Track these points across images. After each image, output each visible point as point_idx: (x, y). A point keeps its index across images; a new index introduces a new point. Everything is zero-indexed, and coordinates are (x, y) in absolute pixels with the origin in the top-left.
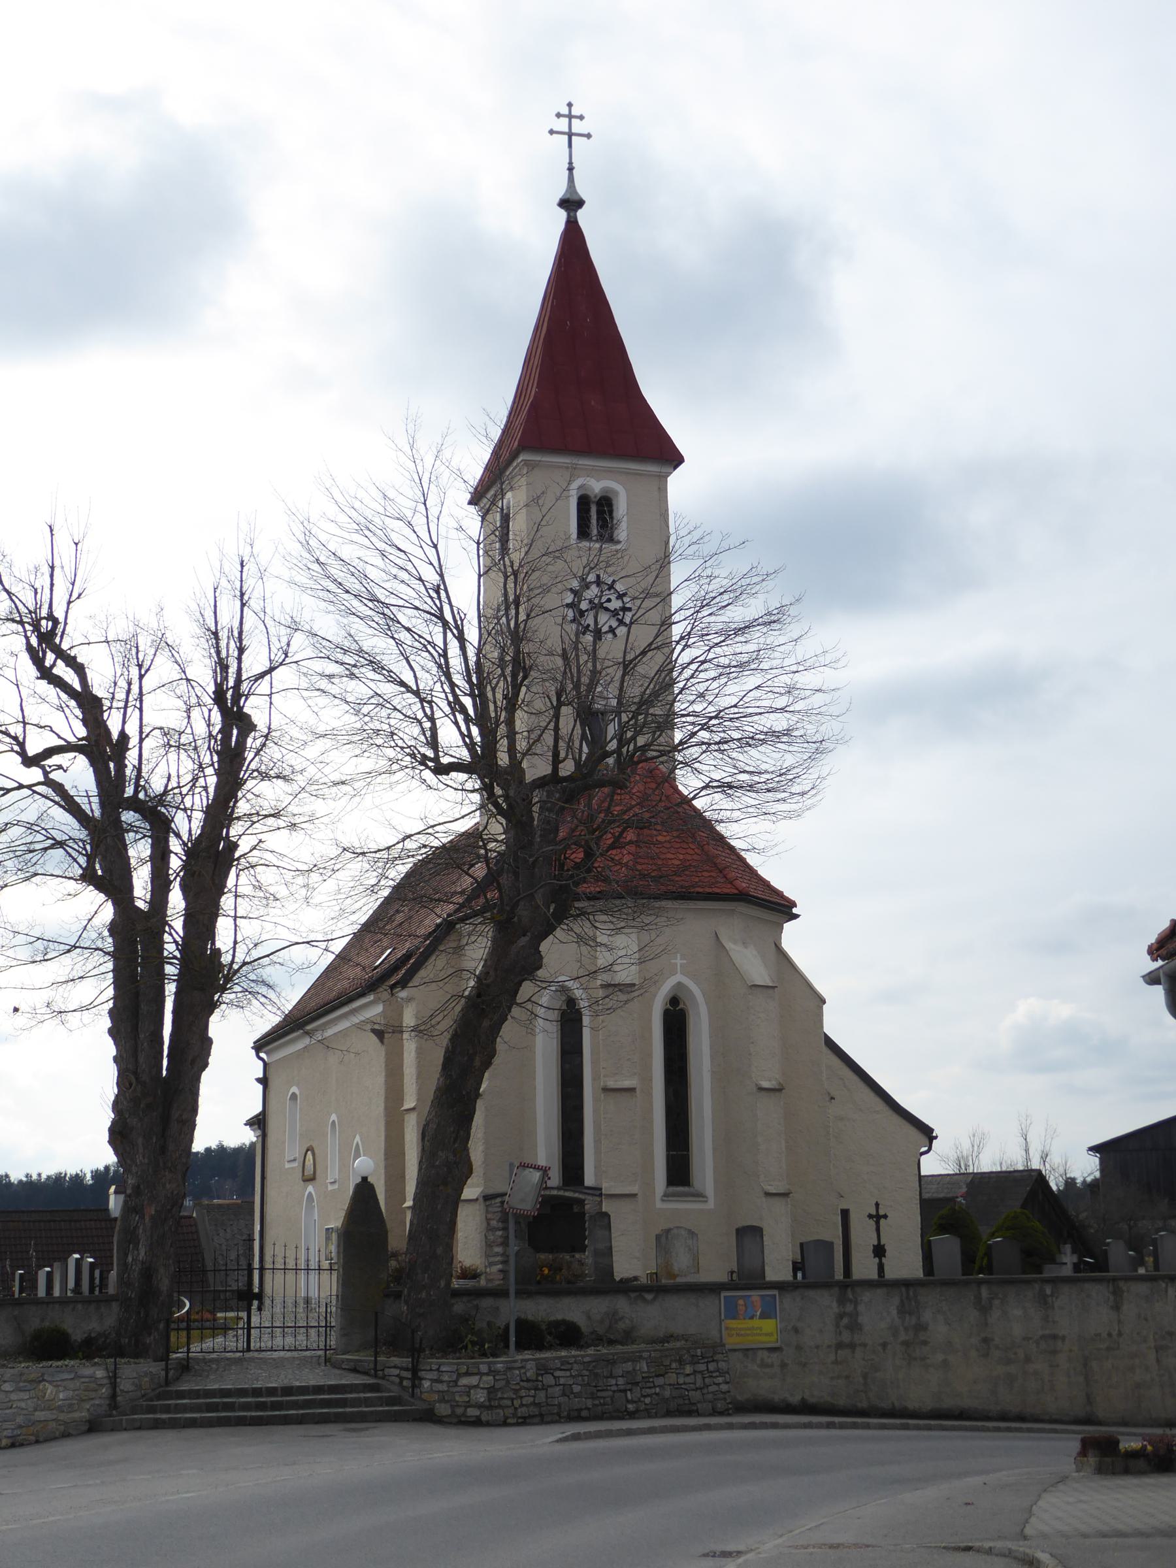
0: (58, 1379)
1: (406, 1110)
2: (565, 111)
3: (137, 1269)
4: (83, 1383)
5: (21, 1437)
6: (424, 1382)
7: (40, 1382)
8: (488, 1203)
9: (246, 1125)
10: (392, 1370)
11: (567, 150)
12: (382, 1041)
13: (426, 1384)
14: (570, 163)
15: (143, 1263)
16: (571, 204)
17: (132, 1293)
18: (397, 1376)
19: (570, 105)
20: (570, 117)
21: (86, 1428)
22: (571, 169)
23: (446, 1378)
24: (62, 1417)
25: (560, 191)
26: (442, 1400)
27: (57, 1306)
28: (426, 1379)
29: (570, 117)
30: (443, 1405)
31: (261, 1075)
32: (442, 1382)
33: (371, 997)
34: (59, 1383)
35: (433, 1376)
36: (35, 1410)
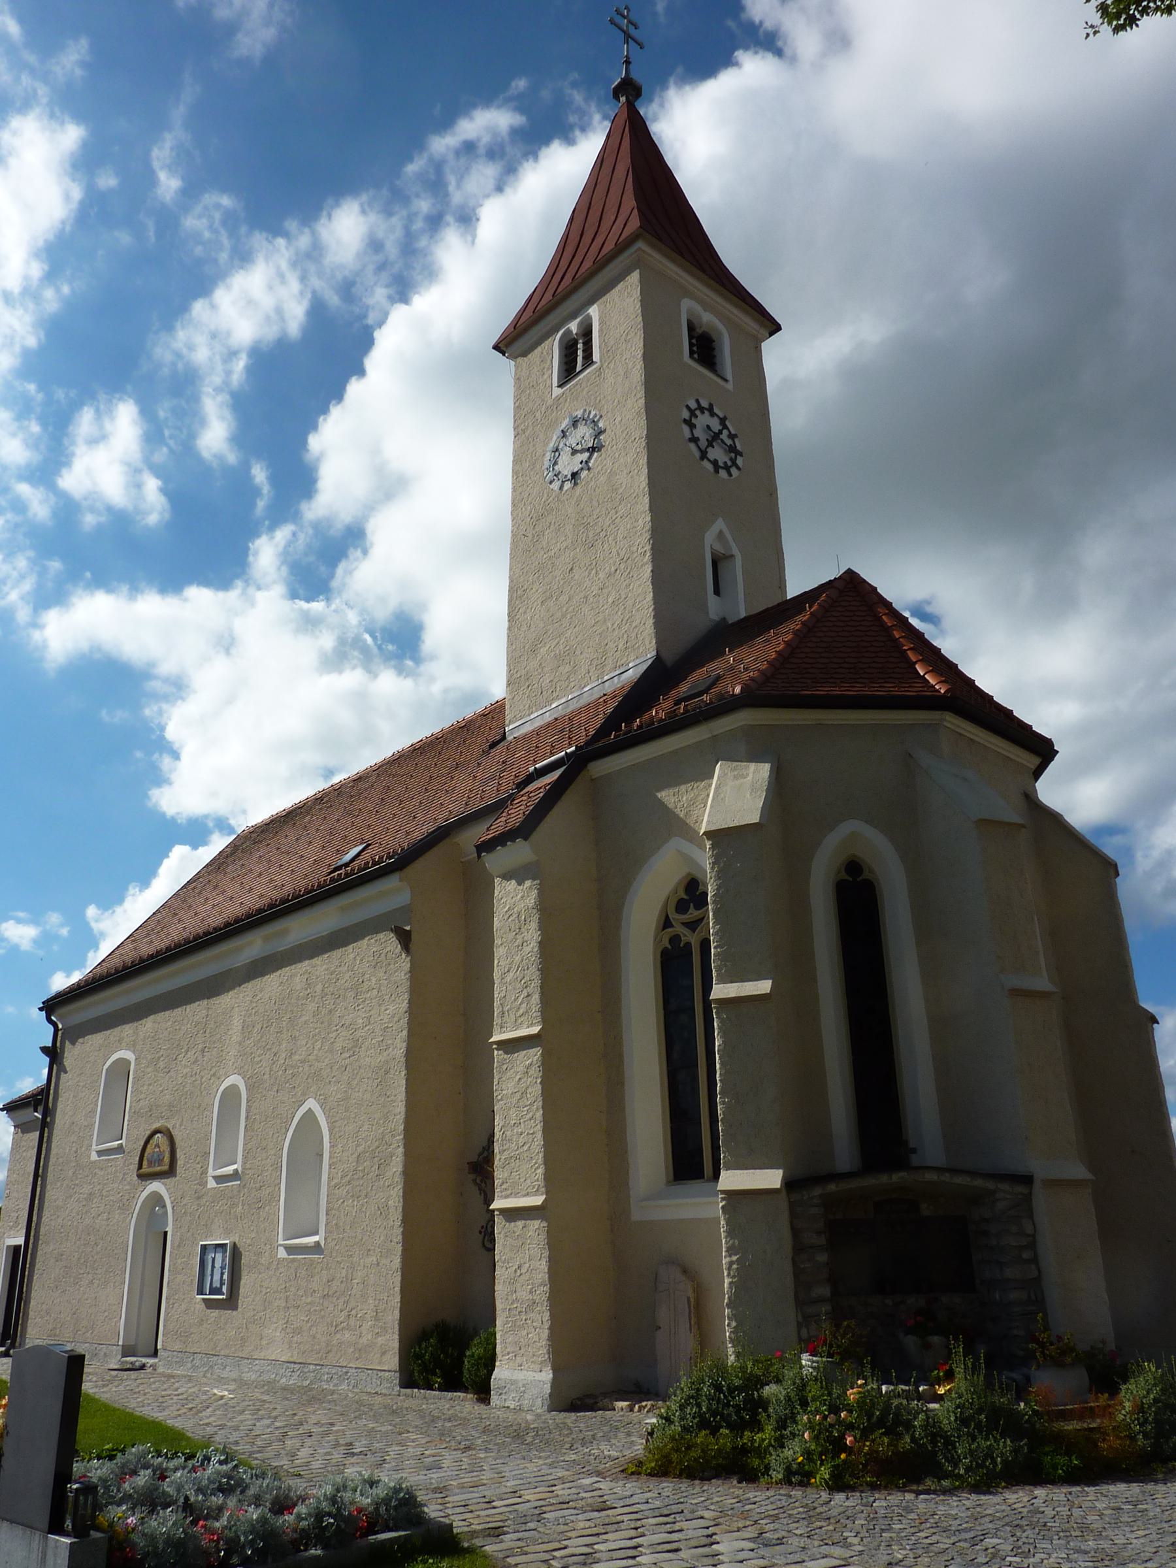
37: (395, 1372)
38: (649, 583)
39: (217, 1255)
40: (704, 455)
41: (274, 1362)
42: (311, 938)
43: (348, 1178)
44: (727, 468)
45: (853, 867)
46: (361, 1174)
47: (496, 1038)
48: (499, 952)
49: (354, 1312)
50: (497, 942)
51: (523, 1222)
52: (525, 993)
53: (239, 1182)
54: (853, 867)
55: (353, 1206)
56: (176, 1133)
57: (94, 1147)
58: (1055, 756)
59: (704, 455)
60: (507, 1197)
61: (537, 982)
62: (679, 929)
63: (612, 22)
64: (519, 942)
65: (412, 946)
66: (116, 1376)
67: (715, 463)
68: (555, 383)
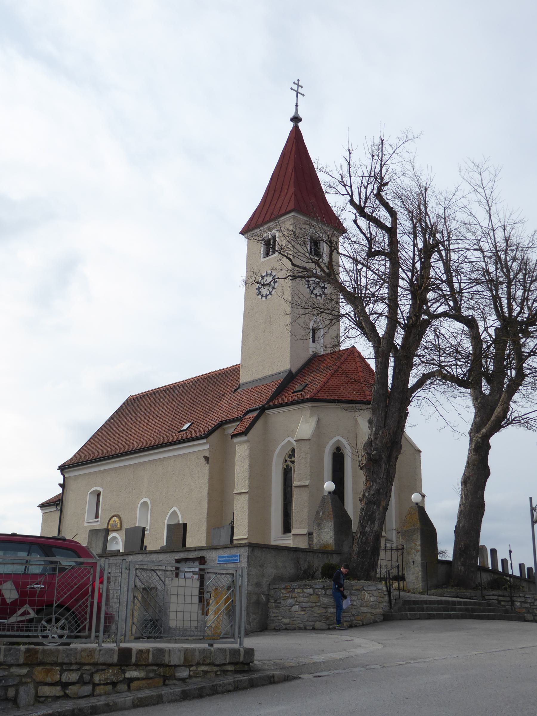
0: (370, 590)
1: (235, 493)
2: (297, 82)
3: (372, 535)
4: (380, 593)
5: (355, 622)
6: (516, 603)
7: (362, 590)
8: (310, 536)
9: (38, 507)
10: (491, 596)
11: (296, 98)
12: (208, 463)
13: (518, 604)
14: (297, 103)
15: (376, 532)
16: (296, 119)
17: (368, 548)
18: (496, 600)
19: (298, 80)
20: (298, 85)
21: (382, 618)
22: (297, 106)
23: (529, 601)
24: (373, 611)
25: (292, 114)
26: (528, 612)
27: (311, 554)
28: (517, 601)
29: (298, 85)
30: (529, 615)
31: (62, 483)
32: (527, 603)
33: (204, 441)
34: (370, 592)
35: (523, 600)
36: (361, 606)
38: (289, 344)
40: (312, 292)
44: (320, 295)
45: (338, 449)
47: (236, 492)
48: (237, 467)
50: (236, 464)
52: (244, 480)
54: (338, 449)
56: (122, 516)
57: (86, 520)
59: (312, 292)
60: (237, 536)
61: (248, 477)
62: (289, 463)
63: (292, 89)
64: (243, 465)
65: (210, 462)
67: (316, 295)
68: (262, 256)
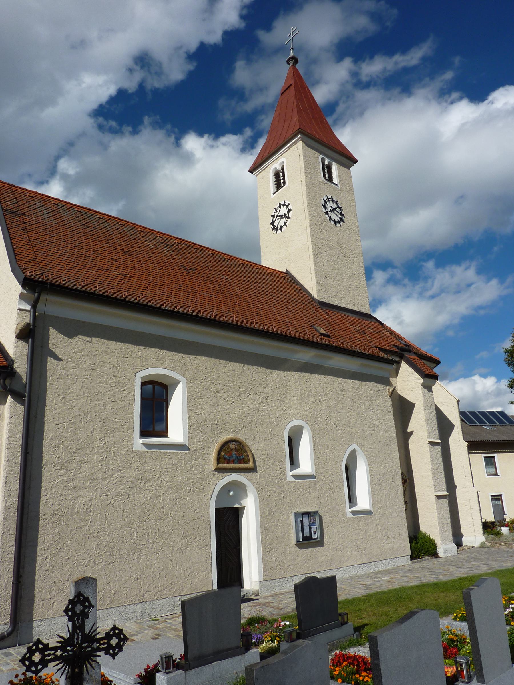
37: (293, 591)
39: (304, 519)
41: (352, 567)
42: (338, 368)
43: (380, 482)
46: (385, 481)
49: (390, 536)
51: (442, 499)
53: (315, 480)
55: (384, 493)
58: (414, 407)
66: (391, 557)
